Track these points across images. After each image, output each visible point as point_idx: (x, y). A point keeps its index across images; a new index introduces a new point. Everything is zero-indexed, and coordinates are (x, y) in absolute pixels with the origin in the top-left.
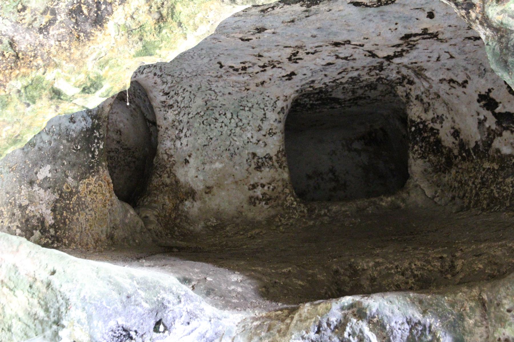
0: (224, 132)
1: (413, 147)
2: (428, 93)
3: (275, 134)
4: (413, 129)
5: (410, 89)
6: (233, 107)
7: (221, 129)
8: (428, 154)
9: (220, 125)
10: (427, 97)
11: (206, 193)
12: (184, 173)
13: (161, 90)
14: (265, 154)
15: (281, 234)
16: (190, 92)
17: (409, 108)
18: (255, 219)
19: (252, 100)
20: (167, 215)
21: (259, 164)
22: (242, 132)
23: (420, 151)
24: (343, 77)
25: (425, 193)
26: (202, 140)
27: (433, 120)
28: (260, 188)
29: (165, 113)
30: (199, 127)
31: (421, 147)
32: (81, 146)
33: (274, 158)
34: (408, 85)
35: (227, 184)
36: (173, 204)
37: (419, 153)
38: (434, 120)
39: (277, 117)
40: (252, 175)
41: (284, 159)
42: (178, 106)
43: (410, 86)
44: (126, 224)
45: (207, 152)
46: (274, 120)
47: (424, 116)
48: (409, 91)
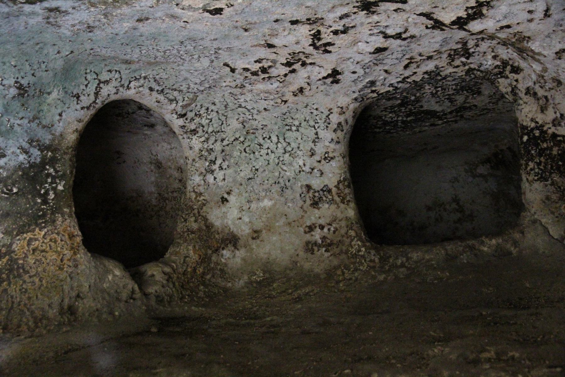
0: (271, 161)
1: (527, 165)
2: (542, 81)
3: (332, 158)
4: (525, 138)
5: (517, 81)
6: (277, 127)
7: (267, 157)
8: (551, 173)
9: (266, 151)
10: (541, 87)
11: (253, 238)
12: (221, 215)
13: (172, 111)
14: (323, 186)
15: (339, 293)
16: (217, 112)
17: (518, 109)
18: (312, 271)
19: (297, 116)
20: (189, 270)
21: (316, 199)
22: (292, 159)
23: (537, 170)
24: (415, 73)
25: (549, 232)
26: (246, 172)
27: (555, 123)
28: (318, 230)
29: (189, 140)
30: (240, 157)
31: (539, 164)
32: (18, 188)
33: (334, 190)
34: (513, 75)
35: (279, 227)
36: (200, 256)
37: (535, 173)
38: (556, 123)
39: (334, 136)
40: (308, 213)
41: (347, 191)
42: (203, 131)
43: (516, 76)
44: (103, 291)
45: (252, 187)
46: (330, 141)
47: (540, 118)
48: (515, 83)
